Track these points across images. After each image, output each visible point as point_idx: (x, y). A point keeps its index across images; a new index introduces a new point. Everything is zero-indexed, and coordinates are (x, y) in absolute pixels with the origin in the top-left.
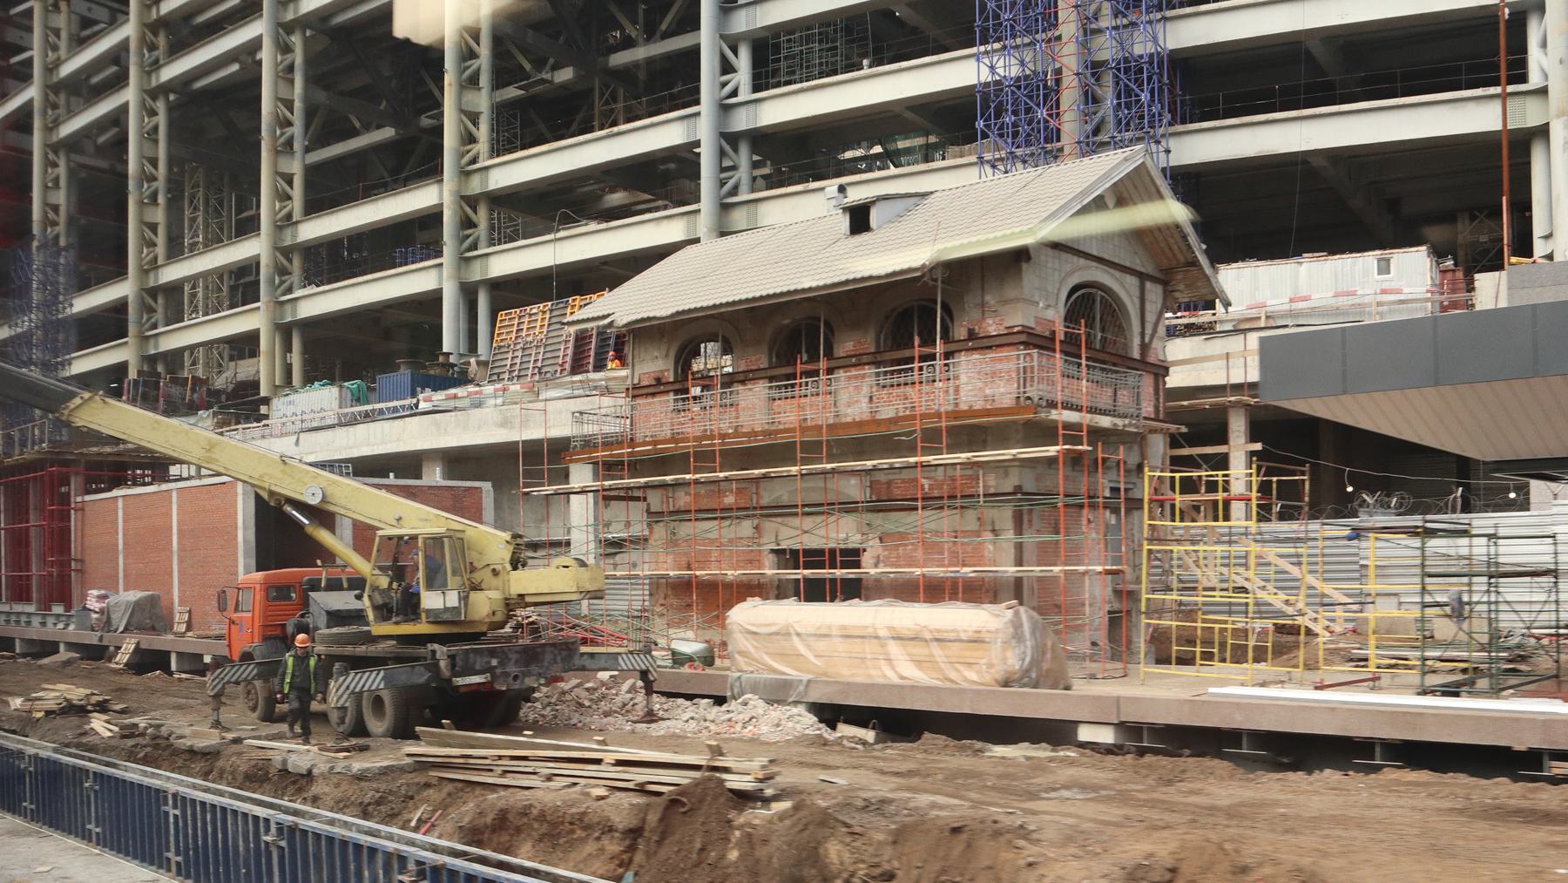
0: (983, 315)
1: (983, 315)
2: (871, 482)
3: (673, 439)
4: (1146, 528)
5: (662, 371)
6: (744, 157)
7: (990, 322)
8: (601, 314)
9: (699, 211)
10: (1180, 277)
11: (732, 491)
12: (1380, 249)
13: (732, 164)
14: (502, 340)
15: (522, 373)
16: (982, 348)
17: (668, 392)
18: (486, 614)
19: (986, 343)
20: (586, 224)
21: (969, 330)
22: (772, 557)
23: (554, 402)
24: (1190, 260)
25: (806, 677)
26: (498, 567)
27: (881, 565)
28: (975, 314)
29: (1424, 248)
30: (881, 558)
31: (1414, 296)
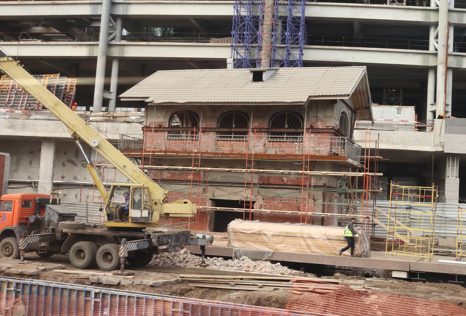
0: (317, 120)
1: (317, 120)
2: (260, 176)
3: (166, 152)
4: (110, 184)
5: (162, 123)
6: (119, 24)
7: (320, 123)
8: (144, 96)
9: (98, 45)
10: (359, 111)
11: (191, 174)
12: (398, 105)
13: (112, 26)
14: (3, 88)
15: (15, 105)
16: (316, 133)
17: (165, 131)
18: (157, 220)
19: (317, 131)
20: (36, 41)
21: (311, 125)
22: (210, 201)
23: (41, 121)
24: (367, 106)
25: (272, 251)
26: (157, 201)
27: (263, 208)
28: (313, 120)
29: (413, 107)
30: (263, 206)
31: (412, 124)
